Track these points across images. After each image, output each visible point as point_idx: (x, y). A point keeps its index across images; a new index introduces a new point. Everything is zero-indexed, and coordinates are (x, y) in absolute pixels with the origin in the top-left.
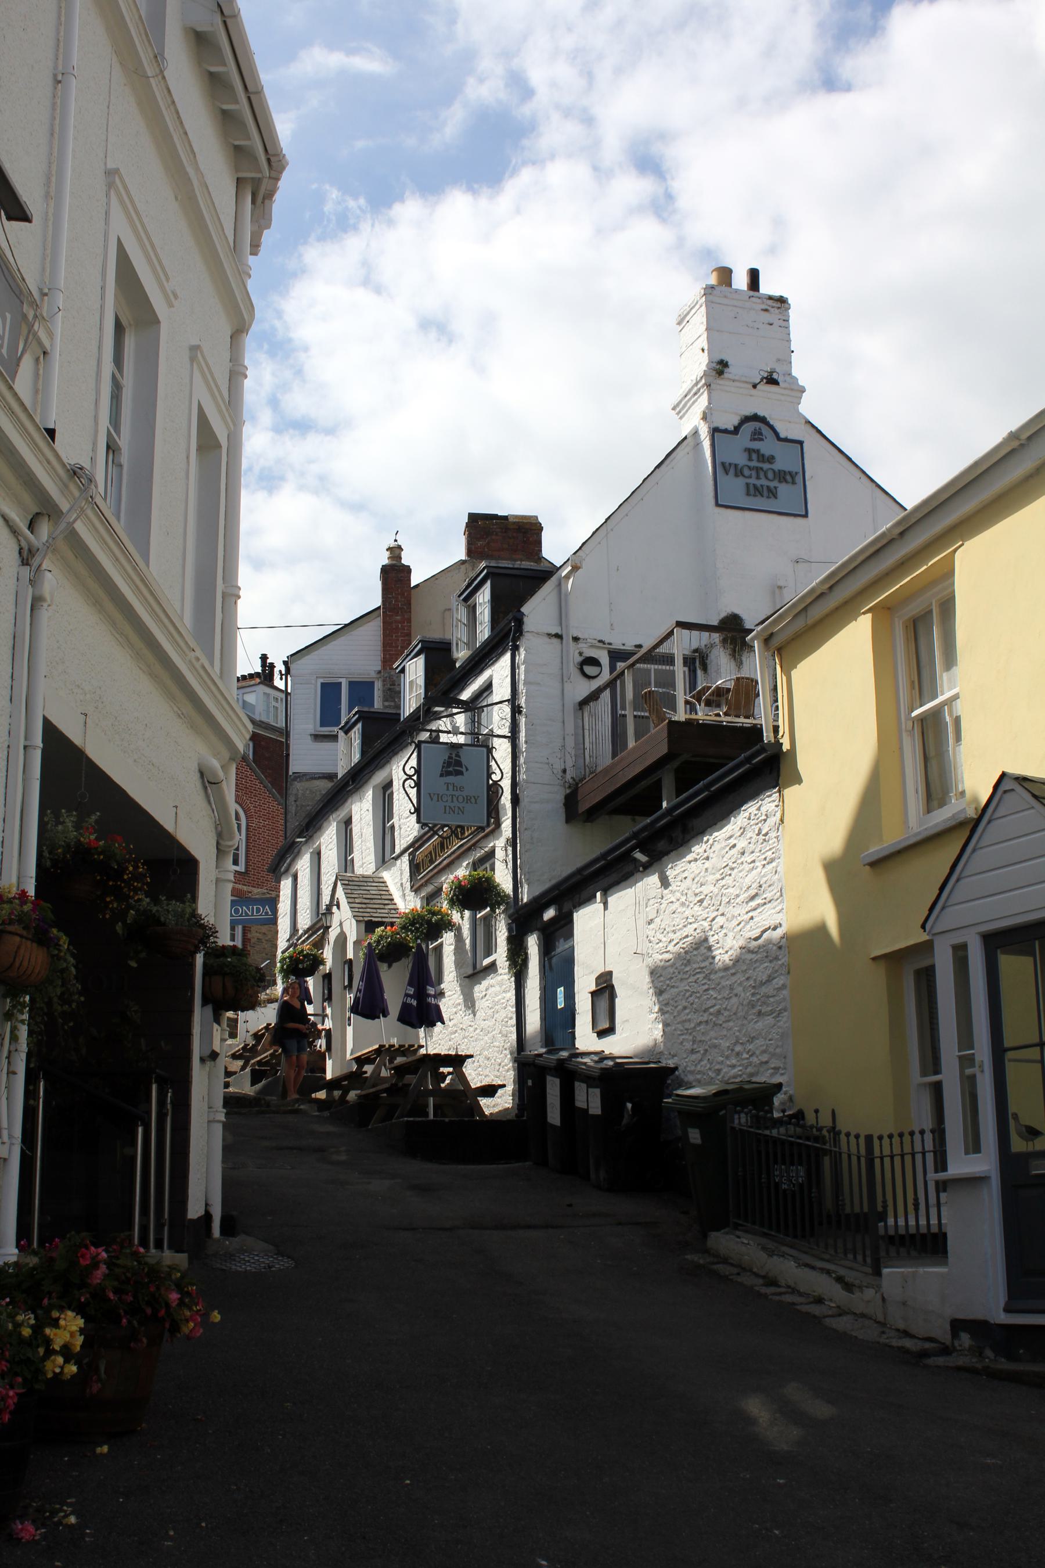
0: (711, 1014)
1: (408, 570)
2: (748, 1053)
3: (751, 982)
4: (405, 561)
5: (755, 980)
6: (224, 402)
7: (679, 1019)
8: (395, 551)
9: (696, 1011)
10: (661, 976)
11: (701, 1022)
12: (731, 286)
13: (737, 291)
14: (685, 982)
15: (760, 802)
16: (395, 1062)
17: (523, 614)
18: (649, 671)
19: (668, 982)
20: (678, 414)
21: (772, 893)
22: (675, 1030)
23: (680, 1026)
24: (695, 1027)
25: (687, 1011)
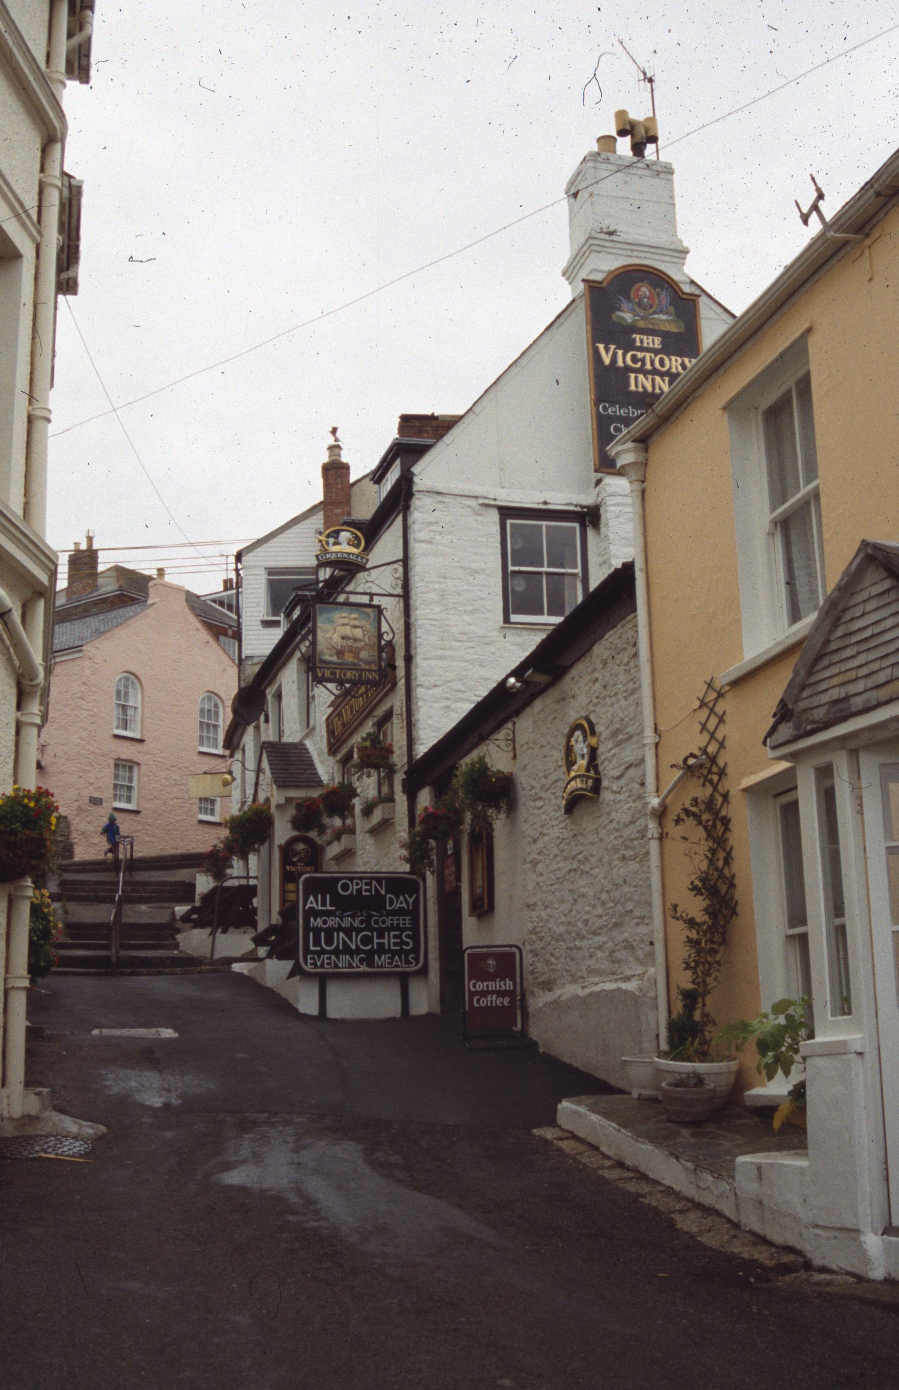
0: (579, 861)
1: (346, 468)
2: (613, 901)
3: (615, 825)
4: (344, 459)
5: (618, 822)
6: (32, 223)
7: (550, 868)
8: (335, 449)
9: (565, 859)
10: (534, 823)
11: (570, 870)
12: (615, 152)
13: (620, 157)
14: (556, 829)
15: (621, 630)
16: (189, 907)
17: (413, 474)
18: (540, 527)
19: (540, 830)
20: (567, 279)
21: (634, 727)
22: (548, 879)
23: (552, 875)
24: (565, 876)
25: (559, 859)
